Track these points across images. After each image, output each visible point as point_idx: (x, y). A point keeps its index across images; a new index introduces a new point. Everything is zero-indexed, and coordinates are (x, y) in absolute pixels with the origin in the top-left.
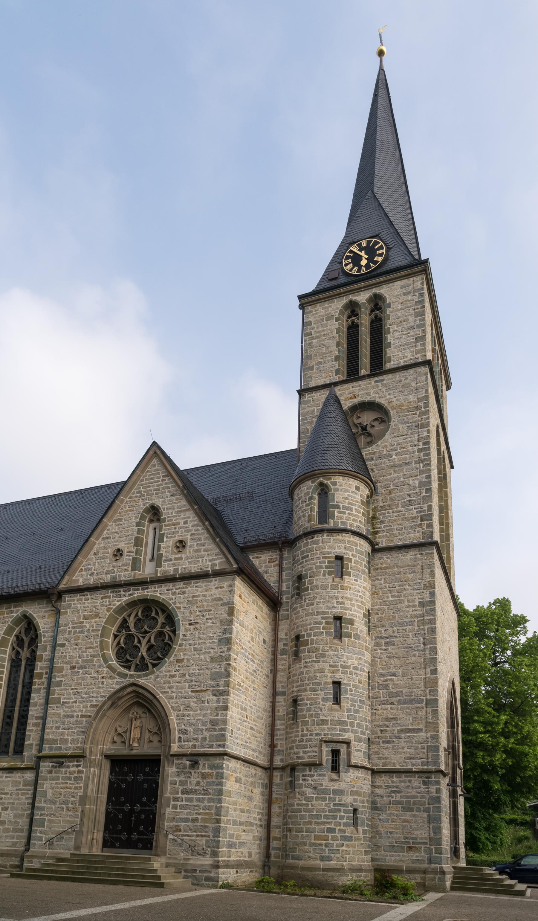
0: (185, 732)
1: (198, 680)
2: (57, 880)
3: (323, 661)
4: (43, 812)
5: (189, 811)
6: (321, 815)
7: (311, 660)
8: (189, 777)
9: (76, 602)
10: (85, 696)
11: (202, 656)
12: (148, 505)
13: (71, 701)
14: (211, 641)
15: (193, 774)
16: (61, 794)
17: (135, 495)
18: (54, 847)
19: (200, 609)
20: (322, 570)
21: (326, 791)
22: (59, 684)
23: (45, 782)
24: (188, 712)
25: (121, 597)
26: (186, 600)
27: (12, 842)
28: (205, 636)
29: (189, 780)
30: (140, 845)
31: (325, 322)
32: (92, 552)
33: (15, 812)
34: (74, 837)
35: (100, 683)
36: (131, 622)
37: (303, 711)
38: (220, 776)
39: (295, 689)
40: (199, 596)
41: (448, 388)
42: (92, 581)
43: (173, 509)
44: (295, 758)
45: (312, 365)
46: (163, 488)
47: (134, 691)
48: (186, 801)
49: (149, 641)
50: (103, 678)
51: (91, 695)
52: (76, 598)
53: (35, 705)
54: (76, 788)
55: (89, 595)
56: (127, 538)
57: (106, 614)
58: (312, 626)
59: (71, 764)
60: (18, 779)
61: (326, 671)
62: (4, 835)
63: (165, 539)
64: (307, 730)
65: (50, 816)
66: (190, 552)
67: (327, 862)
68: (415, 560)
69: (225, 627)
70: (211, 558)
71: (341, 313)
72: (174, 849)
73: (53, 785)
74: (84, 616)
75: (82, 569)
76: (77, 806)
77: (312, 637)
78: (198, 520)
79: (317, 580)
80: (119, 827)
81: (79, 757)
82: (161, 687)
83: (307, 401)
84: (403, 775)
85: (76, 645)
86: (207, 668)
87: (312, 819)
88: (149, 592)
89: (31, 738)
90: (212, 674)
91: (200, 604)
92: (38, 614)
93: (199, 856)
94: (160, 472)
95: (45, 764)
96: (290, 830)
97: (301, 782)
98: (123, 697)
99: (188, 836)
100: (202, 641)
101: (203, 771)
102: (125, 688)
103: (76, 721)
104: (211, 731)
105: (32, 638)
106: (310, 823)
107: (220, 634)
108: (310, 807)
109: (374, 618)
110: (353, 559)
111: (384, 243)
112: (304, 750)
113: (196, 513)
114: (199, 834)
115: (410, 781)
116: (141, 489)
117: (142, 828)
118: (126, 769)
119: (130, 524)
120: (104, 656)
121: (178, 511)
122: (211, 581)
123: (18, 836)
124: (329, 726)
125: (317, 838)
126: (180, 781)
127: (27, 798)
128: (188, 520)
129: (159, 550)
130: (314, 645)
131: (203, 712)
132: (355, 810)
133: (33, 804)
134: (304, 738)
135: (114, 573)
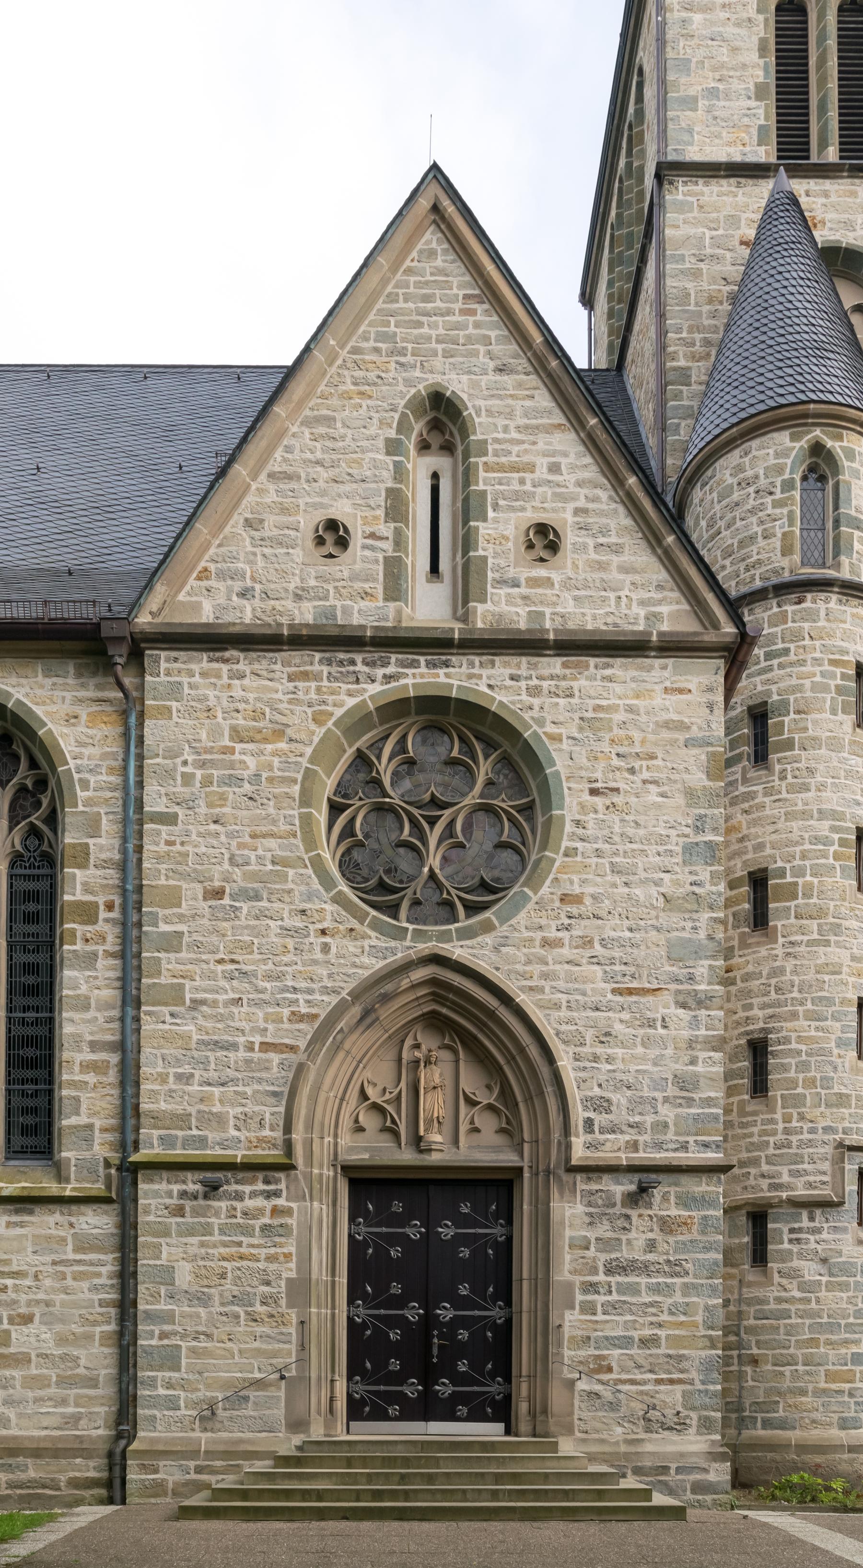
0: (603, 1105)
1: (629, 959)
2: (346, 1518)
4: (167, 1328)
5: (629, 1318)
6: (839, 1325)
7: (805, 938)
8: (624, 1229)
9: (197, 679)
10: (268, 985)
11: (637, 891)
12: (421, 387)
13: (222, 997)
14: (661, 849)
15: (635, 1219)
16: (223, 1276)
17: (372, 344)
18: (218, 1426)
19: (622, 750)
20: (828, 697)
22: (172, 942)
23: (161, 1240)
24: (609, 1051)
25: (357, 681)
26: (576, 716)
27: (63, 1415)
28: (642, 832)
29: (624, 1238)
30: (463, 1410)
32: (237, 519)
33: (58, 1327)
34: (282, 1394)
35: (318, 949)
43: (510, 415)
44: (765, 1187)
45: (692, 92)
46: (469, 339)
47: (433, 982)
48: (619, 1292)
50: (323, 932)
51: (290, 983)
52: (194, 666)
53: (84, 1005)
54: (270, 1259)
55: (243, 661)
56: (360, 487)
57: (313, 733)
58: (807, 846)
59: (247, 1189)
60: (53, 1232)
61: (845, 969)
62: (30, 1394)
63: (491, 514)
64: (802, 1117)
65: (195, 1339)
66: (575, 566)
67: (853, 1431)
69: (702, 811)
72: (594, 1418)
73: (193, 1250)
74: (234, 729)
75: (206, 569)
76: (283, 1309)
77: (808, 878)
78: (595, 468)
79: (815, 722)
80: (395, 1365)
82: (518, 973)
83: (682, 203)
85: (215, 822)
86: (658, 930)
87: (819, 1333)
89: (83, 1108)
90: (670, 945)
91: (621, 732)
92: (53, 708)
93: (666, 1433)
94: (455, 281)
95: (156, 1187)
96: (754, 1361)
97: (786, 1246)
98: (396, 995)
99: (633, 1382)
100: (634, 846)
101: (665, 1213)
102: (406, 967)
103: (248, 1062)
104: (680, 1105)
105: (22, 789)
106: (813, 1342)
107: (687, 831)
108: (813, 1305)
112: (793, 1167)
113: (591, 443)
114: (664, 1376)
116: (393, 328)
117: (462, 1367)
118: (397, 1207)
119: (364, 443)
121: (527, 427)
122: (650, 669)
123: (78, 1397)
124: (853, 1110)
125: (830, 1377)
126: (597, 1239)
127: (95, 1289)
128: (564, 462)
130: (814, 900)
131: (653, 1053)
134: (794, 1139)
135: (326, 598)
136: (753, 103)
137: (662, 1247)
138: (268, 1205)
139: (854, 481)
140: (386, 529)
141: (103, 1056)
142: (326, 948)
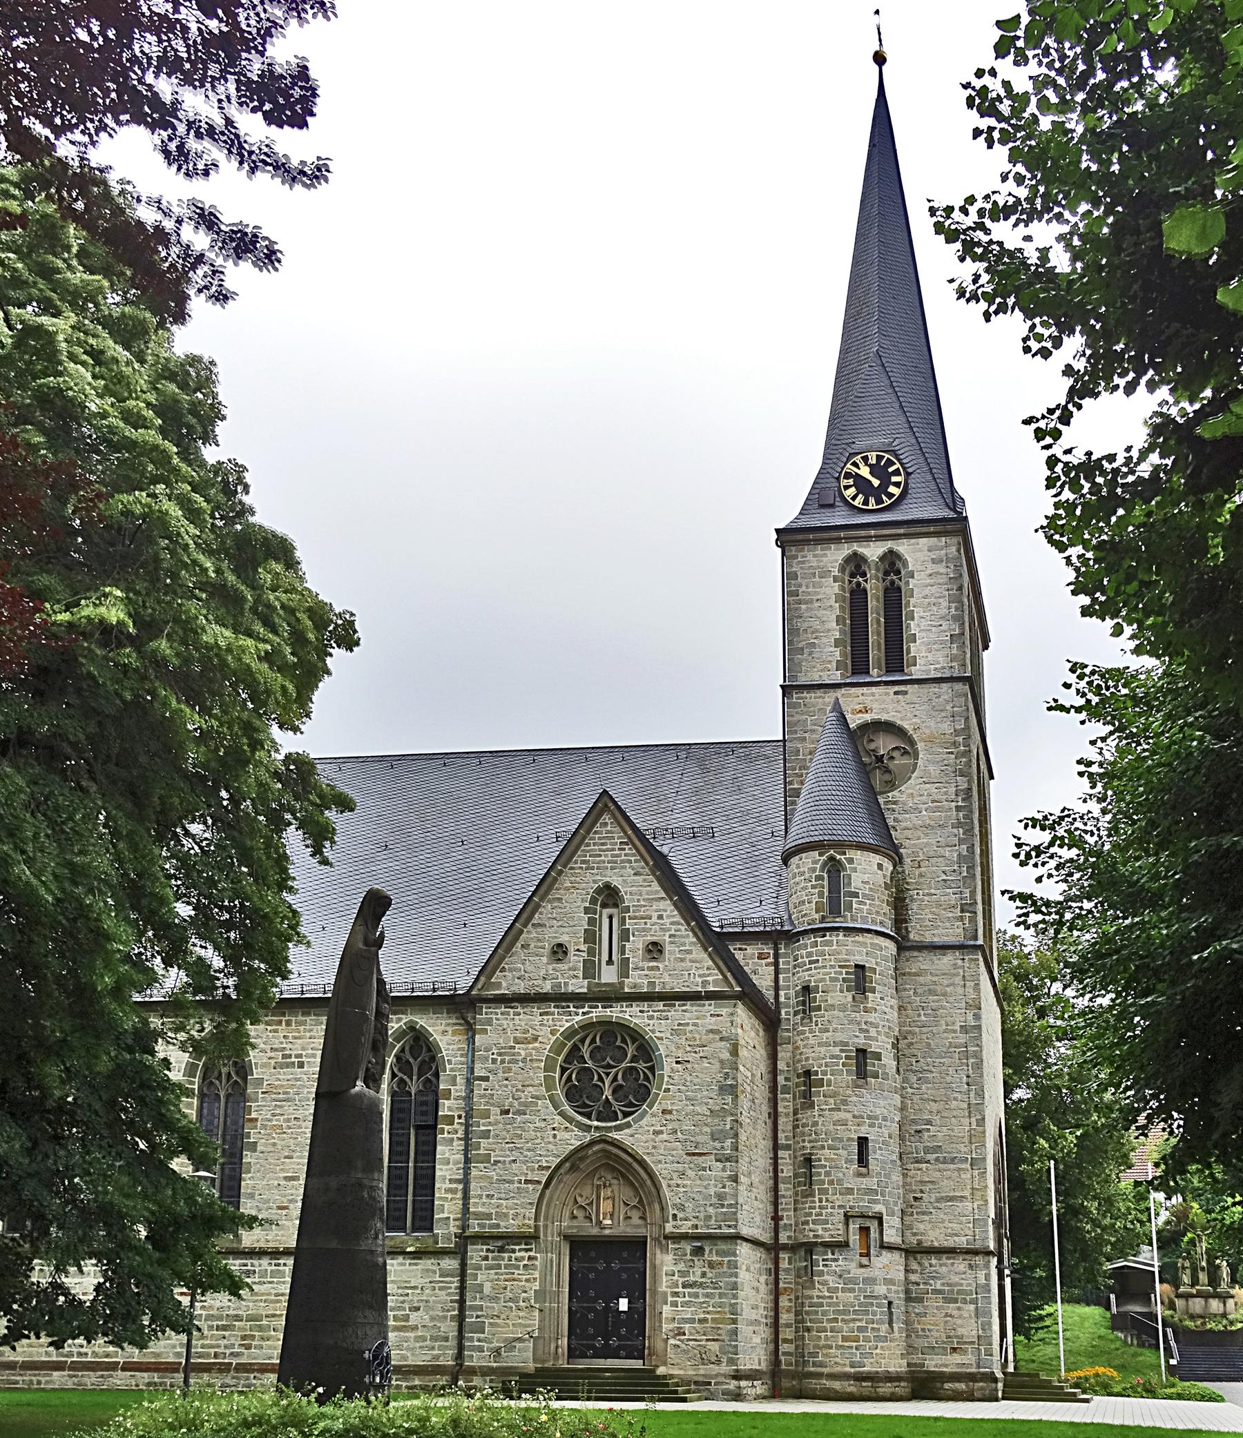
3: (845, 1111)
16: (505, 1288)
21: (854, 1281)
22: (486, 1135)
31: (817, 579)
32: (519, 945)
33: (431, 1313)
36: (585, 1051)
37: (820, 1174)
38: (734, 1265)
39: (808, 1145)
40: (688, 1024)
41: (986, 647)
42: (521, 988)
43: (641, 895)
46: (622, 862)
47: (603, 1150)
49: (615, 1079)
54: (527, 1280)
59: (517, 1248)
62: (418, 1345)
68: (955, 966)
70: (701, 972)
71: (842, 569)
73: (492, 1277)
81: (528, 1239)
84: (945, 1256)
88: (616, 1012)
96: (808, 1330)
109: (902, 1044)
110: (878, 969)
111: (902, 464)
115: (953, 1264)
120: (552, 1098)
125: (845, 1339)
129: (623, 953)
132: (890, 1303)
133: (462, 1302)
136: (833, 649)
137: (709, 1275)
138: (526, 1255)
139: (853, 874)
140: (584, 947)
141: (454, 1186)
142: (555, 1136)
